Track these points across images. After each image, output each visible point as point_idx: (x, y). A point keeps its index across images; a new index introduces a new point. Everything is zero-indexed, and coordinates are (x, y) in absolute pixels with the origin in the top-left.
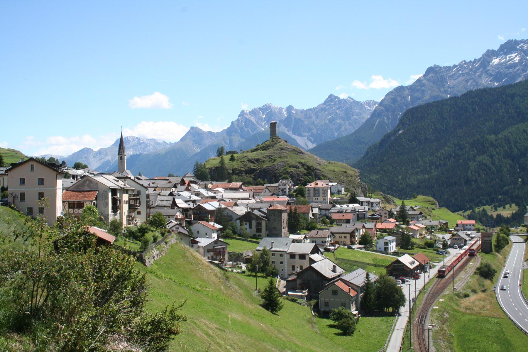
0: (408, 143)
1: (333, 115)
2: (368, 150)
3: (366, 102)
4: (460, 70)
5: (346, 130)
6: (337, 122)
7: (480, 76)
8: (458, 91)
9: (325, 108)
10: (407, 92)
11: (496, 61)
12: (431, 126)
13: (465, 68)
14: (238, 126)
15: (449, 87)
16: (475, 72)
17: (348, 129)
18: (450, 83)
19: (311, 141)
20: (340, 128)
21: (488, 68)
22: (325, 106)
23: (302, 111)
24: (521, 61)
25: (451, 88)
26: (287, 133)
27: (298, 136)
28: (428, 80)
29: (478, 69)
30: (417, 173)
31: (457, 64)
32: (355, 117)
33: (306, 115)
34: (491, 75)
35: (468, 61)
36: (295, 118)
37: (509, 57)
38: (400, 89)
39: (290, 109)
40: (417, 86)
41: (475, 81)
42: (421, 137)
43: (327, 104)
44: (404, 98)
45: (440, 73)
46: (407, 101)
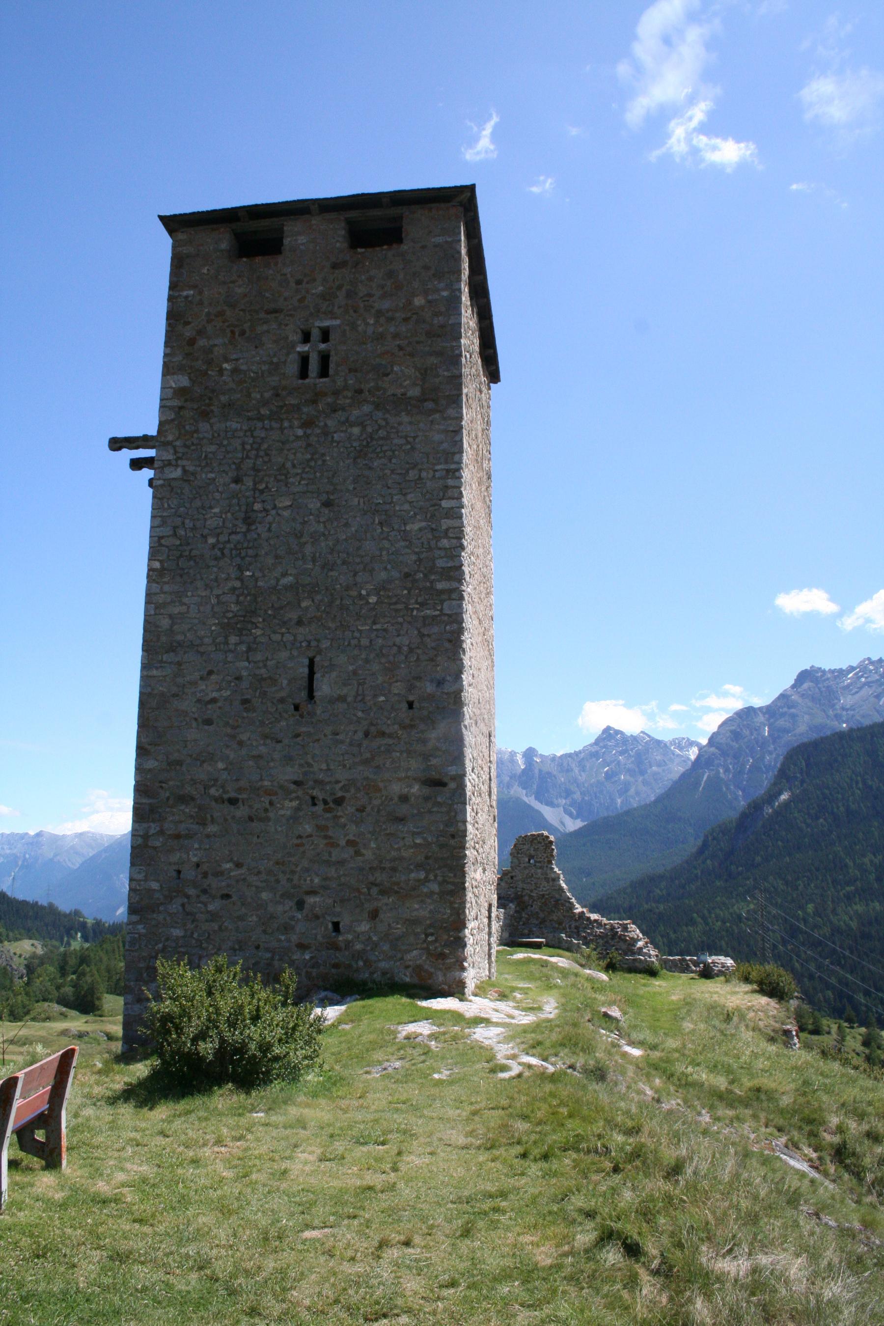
0: (809, 821)
2: (706, 836)
3: (673, 742)
4: (862, 676)
5: (638, 793)
6: (620, 779)
8: (863, 716)
9: (597, 752)
10: (761, 718)
12: (857, 783)
13: (871, 671)
15: (843, 709)
17: (643, 793)
18: (846, 700)
19: (571, 815)
20: (627, 790)
22: (596, 748)
23: (554, 758)
25: (847, 710)
26: (526, 799)
27: (547, 805)
30: (849, 898)
31: (855, 665)
33: (561, 765)
35: (875, 658)
36: (540, 771)
38: (747, 713)
39: (530, 754)
40: (782, 707)
42: (838, 808)
43: (601, 744)
44: (756, 730)
45: (825, 680)
46: (763, 737)
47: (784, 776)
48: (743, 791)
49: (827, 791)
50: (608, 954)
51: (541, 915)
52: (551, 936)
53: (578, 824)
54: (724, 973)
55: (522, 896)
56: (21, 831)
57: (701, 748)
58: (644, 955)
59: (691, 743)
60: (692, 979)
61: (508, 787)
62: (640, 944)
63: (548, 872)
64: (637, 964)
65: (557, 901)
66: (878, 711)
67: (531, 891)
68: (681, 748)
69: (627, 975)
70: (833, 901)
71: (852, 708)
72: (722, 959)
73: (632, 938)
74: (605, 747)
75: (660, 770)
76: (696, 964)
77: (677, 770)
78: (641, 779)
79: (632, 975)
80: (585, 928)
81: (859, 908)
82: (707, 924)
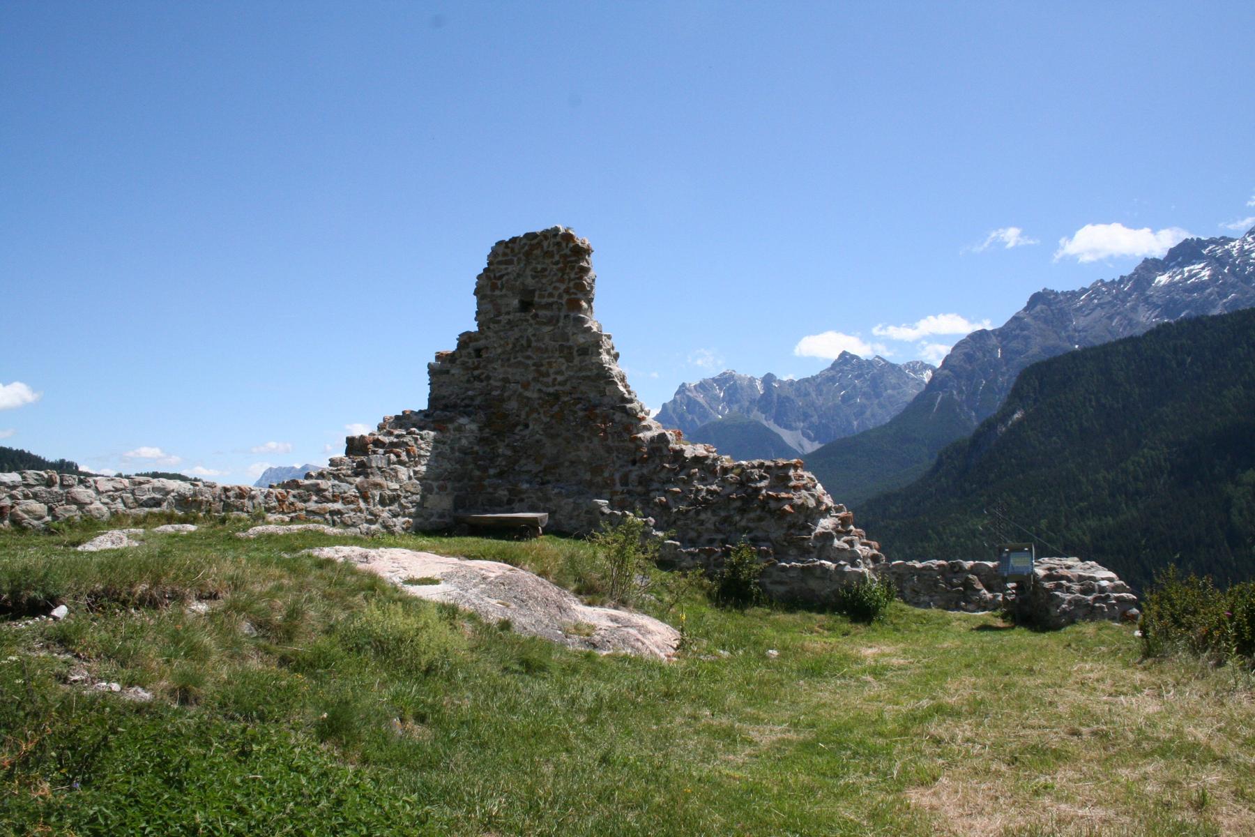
1: (849, 389)
2: (940, 455)
3: (907, 366)
5: (873, 415)
7: (1134, 309)
8: (1095, 337)
11: (1163, 279)
12: (1090, 401)
14: (674, 410)
15: (1075, 330)
16: (1124, 301)
17: (879, 415)
18: (1078, 322)
19: (809, 438)
21: (1148, 293)
22: (833, 373)
23: (791, 383)
24: (1213, 277)
26: (765, 423)
28: (1035, 318)
29: (1129, 294)
32: (889, 391)
33: (798, 390)
34: (1156, 306)
35: (1107, 280)
37: (1190, 271)
39: (768, 379)
41: (1125, 317)
46: (996, 358)
47: (1017, 395)
48: (976, 412)
49: (1060, 410)
50: (727, 553)
51: (550, 449)
52: (567, 504)
53: (817, 446)
54: (1091, 608)
55: (501, 400)
56: (288, 465)
57: (934, 371)
58: (836, 555)
59: (925, 367)
60: (985, 628)
61: (748, 412)
62: (826, 524)
63: (570, 330)
64: (813, 584)
65: (591, 408)
66: (1110, 332)
67: (526, 386)
68: (915, 372)
69: (782, 617)
70: (1066, 517)
71: (1084, 330)
72: (1075, 566)
73: (802, 508)
74: (841, 371)
75: (895, 393)
76: (993, 581)
77: (912, 392)
78: (876, 402)
79: (797, 617)
80: (668, 481)
81: (1093, 523)
82: (941, 539)
